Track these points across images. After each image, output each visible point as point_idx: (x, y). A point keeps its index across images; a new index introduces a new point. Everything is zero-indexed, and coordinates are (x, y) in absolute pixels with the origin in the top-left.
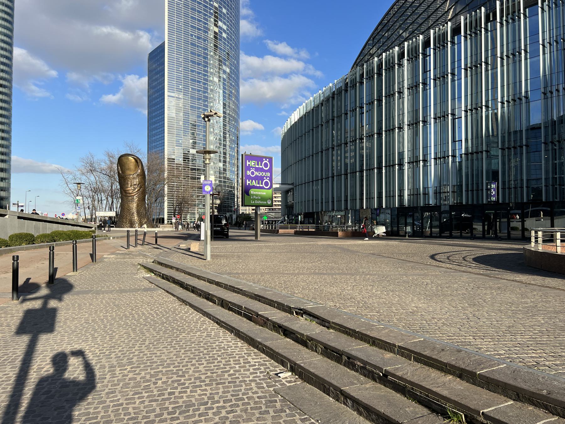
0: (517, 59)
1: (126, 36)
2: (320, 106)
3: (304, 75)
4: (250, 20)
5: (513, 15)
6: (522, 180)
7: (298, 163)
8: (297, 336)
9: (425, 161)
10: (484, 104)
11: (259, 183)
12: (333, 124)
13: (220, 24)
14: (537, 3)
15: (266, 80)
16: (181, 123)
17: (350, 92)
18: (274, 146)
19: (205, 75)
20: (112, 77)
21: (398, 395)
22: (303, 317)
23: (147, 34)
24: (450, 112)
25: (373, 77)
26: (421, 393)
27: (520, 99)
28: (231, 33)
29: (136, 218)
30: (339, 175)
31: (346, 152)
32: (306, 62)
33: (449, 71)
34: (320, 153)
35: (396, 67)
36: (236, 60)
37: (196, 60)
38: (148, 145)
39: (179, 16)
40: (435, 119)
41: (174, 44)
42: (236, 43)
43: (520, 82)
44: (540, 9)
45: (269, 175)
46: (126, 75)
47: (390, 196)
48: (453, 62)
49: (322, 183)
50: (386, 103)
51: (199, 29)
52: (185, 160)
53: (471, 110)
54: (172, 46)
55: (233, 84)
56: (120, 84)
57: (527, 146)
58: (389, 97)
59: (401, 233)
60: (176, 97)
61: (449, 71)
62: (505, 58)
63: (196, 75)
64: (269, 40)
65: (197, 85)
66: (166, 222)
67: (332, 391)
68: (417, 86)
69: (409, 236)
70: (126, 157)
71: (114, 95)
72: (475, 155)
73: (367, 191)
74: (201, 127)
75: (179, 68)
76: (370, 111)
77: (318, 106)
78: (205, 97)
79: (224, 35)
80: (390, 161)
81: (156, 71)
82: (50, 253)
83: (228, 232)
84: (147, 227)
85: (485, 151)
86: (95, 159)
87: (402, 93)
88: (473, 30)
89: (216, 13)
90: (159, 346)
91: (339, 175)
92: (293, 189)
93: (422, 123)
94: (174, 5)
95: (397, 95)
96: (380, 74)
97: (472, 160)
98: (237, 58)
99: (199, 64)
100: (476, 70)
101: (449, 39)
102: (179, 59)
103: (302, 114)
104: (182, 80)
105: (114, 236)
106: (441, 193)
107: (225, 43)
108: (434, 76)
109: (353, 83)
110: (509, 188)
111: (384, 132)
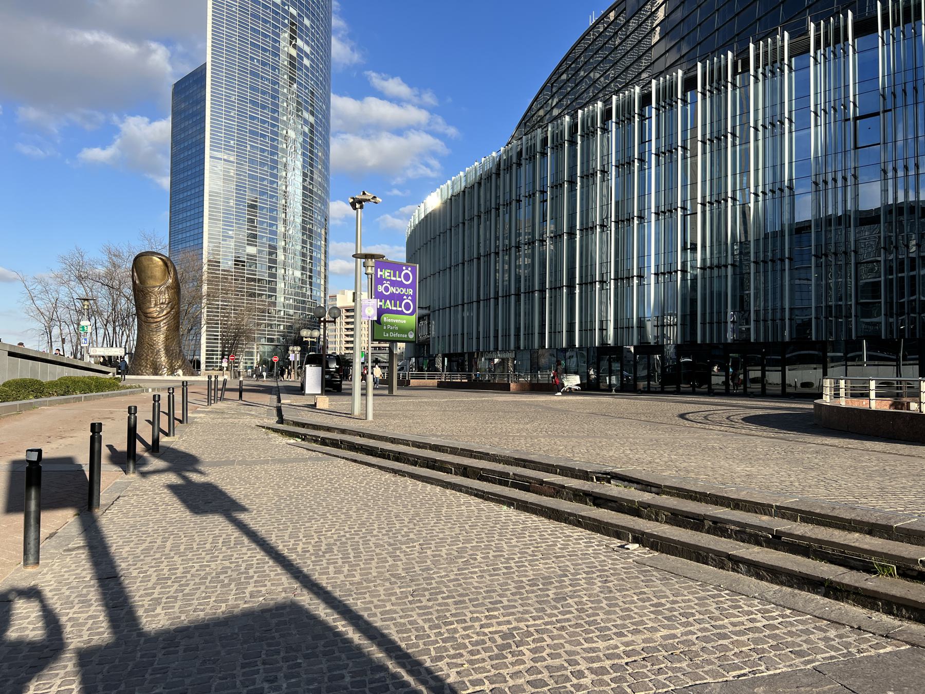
0: (778, 130)
1: (126, 49)
2: (476, 185)
3: (429, 132)
4: (340, 36)
5: (773, 66)
6: (783, 309)
7: (437, 274)
8: (621, 505)
9: (641, 277)
10: (730, 195)
11: (395, 306)
12: (498, 215)
13: (300, 43)
14: (809, 51)
15: (367, 136)
16: (232, 203)
17: (526, 168)
18: (379, 244)
19: (273, 126)
20: (101, 117)
21: (799, 557)
22: (610, 483)
23: (164, 48)
24: (679, 205)
25: (562, 145)
26: (833, 550)
27: (781, 190)
28: (318, 59)
29: (163, 359)
30: (506, 296)
31: (517, 258)
32: (432, 110)
33: (679, 144)
34: (475, 261)
35: (599, 133)
36: (324, 103)
37: (258, 100)
38: (170, 237)
39: (230, 26)
40: (657, 214)
41: (222, 72)
42: (325, 75)
43: (782, 165)
44: (812, 60)
45: (411, 293)
46: (125, 115)
47: (587, 329)
48: (684, 131)
49: (478, 308)
50: (582, 187)
51: (265, 50)
52: (238, 265)
53: (711, 203)
54: (218, 74)
55: (320, 142)
56: (117, 130)
57: (790, 259)
58: (588, 179)
59: (602, 386)
60: (225, 160)
61: (679, 144)
62: (760, 128)
63: (258, 125)
64: (375, 71)
65: (261, 140)
66: (203, 366)
67: (712, 558)
68: (630, 163)
69: (616, 391)
70: (147, 257)
71: (104, 148)
72: (716, 270)
73: (550, 321)
74: (265, 210)
75: (230, 112)
76: (556, 199)
77: (472, 187)
78: (273, 161)
79: (306, 62)
80: (587, 276)
81: (187, 113)
82: (154, 405)
83: (341, 381)
84: (184, 374)
85: (731, 265)
86: (86, 258)
87: (607, 172)
88: (715, 84)
89: (292, 24)
90: (25, 611)
91: (506, 296)
92: (429, 315)
93: (638, 220)
94: (224, 8)
95: (599, 175)
96: (573, 143)
97: (711, 278)
98: (327, 102)
99: (264, 107)
100: (719, 145)
101: (679, 96)
102: (230, 97)
103: (446, 198)
104: (234, 132)
105: (154, 387)
106: (664, 326)
107: (307, 75)
108: (656, 149)
109: (531, 153)
110: (765, 321)
111: (578, 232)
